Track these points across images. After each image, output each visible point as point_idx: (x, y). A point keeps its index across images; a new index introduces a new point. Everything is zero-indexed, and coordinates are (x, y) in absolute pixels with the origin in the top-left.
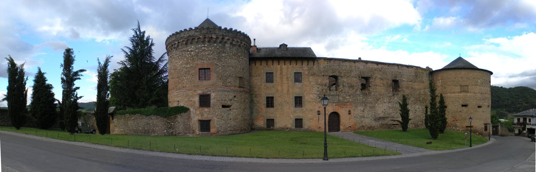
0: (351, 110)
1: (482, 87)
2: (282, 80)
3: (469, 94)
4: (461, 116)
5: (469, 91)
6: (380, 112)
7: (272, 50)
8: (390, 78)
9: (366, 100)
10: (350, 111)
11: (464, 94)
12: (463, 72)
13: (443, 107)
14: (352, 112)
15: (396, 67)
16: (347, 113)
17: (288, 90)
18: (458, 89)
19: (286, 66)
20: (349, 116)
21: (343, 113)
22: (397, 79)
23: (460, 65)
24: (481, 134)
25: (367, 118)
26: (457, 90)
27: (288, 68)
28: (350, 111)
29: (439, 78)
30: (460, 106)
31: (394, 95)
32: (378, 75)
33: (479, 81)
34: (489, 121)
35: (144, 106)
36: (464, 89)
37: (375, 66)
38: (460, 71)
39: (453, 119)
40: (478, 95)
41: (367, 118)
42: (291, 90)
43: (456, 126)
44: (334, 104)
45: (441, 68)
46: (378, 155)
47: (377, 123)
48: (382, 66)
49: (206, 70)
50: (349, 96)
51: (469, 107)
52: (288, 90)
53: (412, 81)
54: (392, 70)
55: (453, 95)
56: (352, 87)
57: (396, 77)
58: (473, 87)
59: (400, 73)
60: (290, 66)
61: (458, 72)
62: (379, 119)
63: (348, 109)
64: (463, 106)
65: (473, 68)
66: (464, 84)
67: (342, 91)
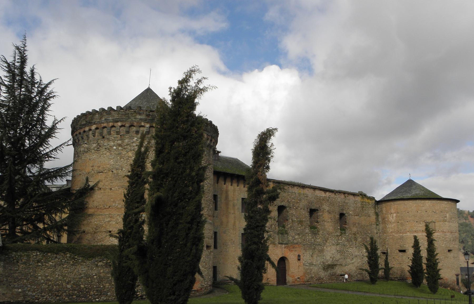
0: (300, 254)
1: (451, 224)
2: (228, 208)
6: (328, 258)
8: (337, 210)
9: (315, 241)
10: (299, 256)
12: (428, 203)
14: (302, 257)
16: (296, 258)
17: (235, 222)
19: (232, 187)
20: (298, 263)
21: (292, 257)
22: (345, 212)
23: (414, 193)
25: (315, 265)
26: (419, 228)
27: (234, 191)
28: (299, 256)
29: (393, 211)
31: (342, 233)
32: (326, 207)
33: (448, 215)
34: (459, 272)
35: (57, 170)
37: (322, 194)
38: (423, 201)
41: (315, 265)
42: (237, 223)
44: (283, 246)
47: (326, 273)
48: (330, 194)
50: (298, 234)
52: (235, 222)
56: (301, 222)
57: (343, 210)
60: (237, 188)
62: (328, 268)
63: (297, 254)
65: (432, 197)
67: (291, 227)
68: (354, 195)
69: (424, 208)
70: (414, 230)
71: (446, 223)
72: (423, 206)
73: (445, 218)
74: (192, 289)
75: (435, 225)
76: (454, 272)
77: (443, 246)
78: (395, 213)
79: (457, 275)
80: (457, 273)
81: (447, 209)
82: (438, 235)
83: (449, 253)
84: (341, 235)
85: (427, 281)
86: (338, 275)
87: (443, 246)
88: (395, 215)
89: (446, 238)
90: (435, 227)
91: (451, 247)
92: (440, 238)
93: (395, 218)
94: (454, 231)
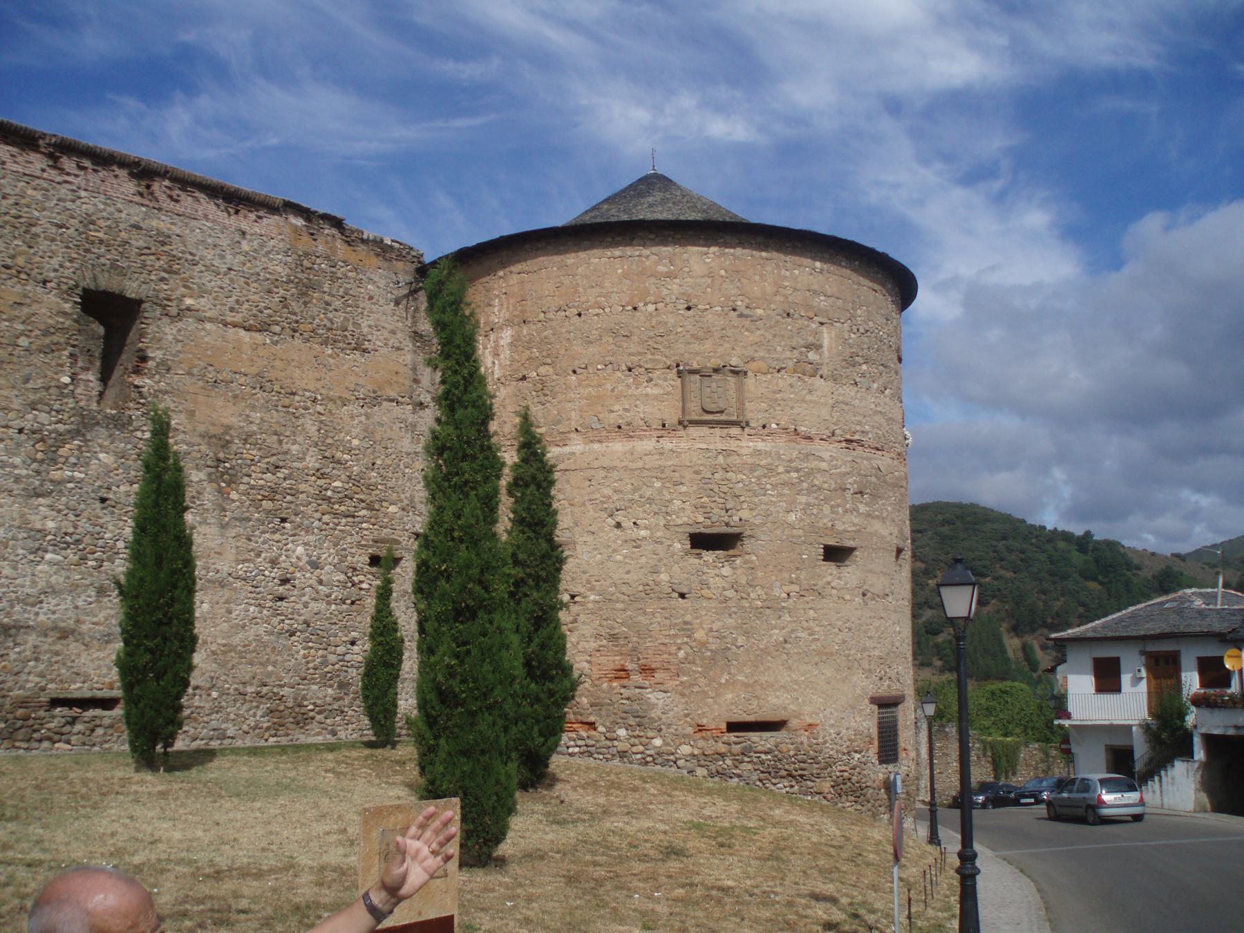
1: (848, 391)
3: (747, 445)
4: (687, 628)
5: (754, 412)
7: (741, 244)
11: (713, 439)
13: (542, 556)
15: (128, 186)
18: (658, 397)
22: (132, 288)
24: (849, 788)
30: (680, 545)
33: (827, 338)
34: (902, 676)
36: (709, 399)
39: (610, 661)
40: (828, 451)
43: (641, 721)
45: (559, 223)
46: (712, 413)
49: (327, 241)
51: (755, 549)
53: (263, 328)
54: (88, 204)
55: (618, 446)
58: (783, 380)
59: (164, 239)
61: (655, 257)
64: (702, 541)
66: (703, 354)
68: (1029, 876)
69: (674, 286)
70: (613, 419)
71: (818, 382)
72: (671, 275)
73: (812, 356)
74: (396, 713)
75: (740, 389)
76: (865, 685)
77: (792, 517)
78: (509, 323)
79: (886, 704)
80: (885, 689)
81: (821, 302)
82: (758, 453)
83: (830, 570)
84: (77, 433)
85: (1062, 792)
86: (23, 703)
87: (792, 517)
88: (507, 335)
89: (811, 473)
90: (741, 401)
91: (845, 528)
92: (770, 469)
93: (506, 354)
94: (869, 439)
